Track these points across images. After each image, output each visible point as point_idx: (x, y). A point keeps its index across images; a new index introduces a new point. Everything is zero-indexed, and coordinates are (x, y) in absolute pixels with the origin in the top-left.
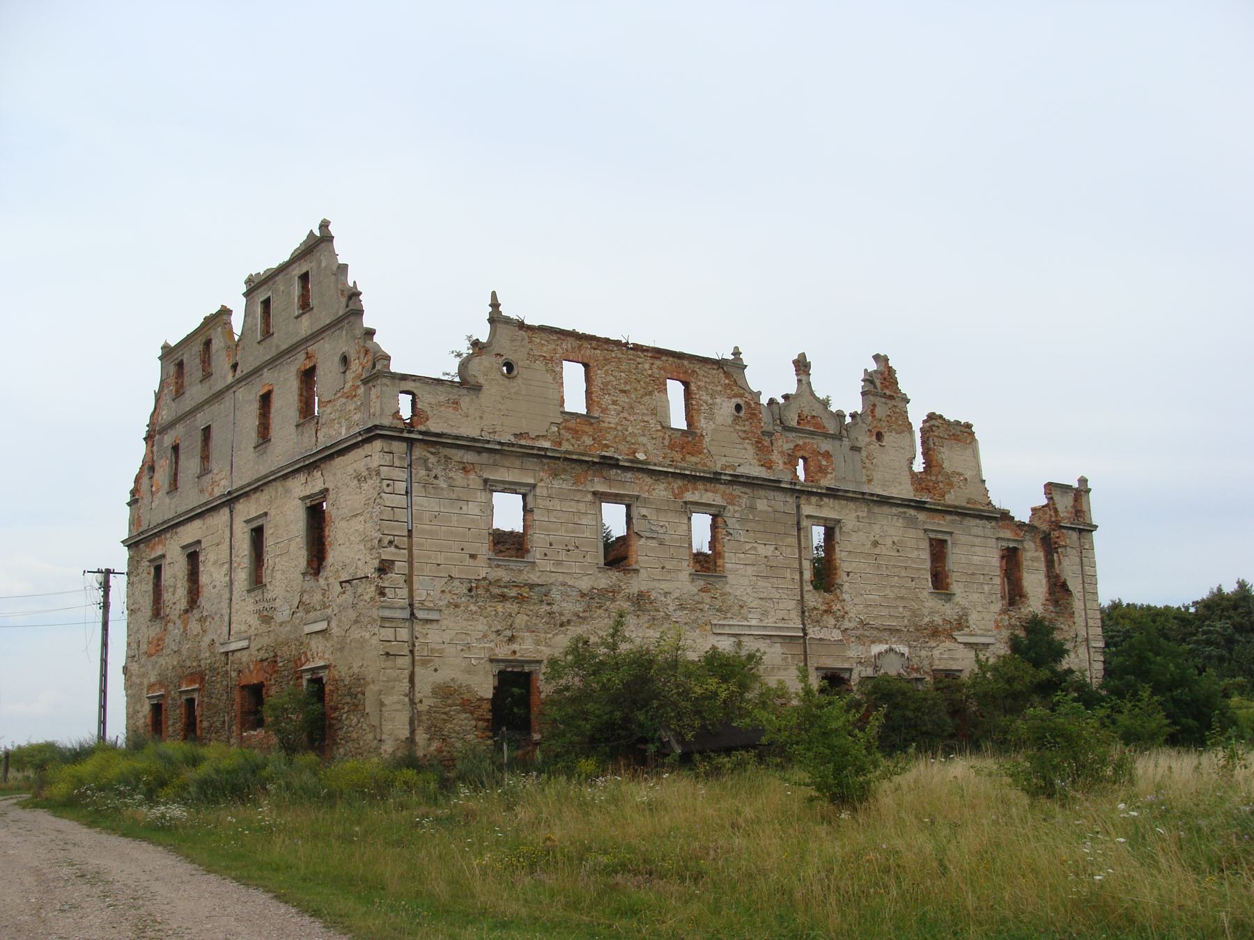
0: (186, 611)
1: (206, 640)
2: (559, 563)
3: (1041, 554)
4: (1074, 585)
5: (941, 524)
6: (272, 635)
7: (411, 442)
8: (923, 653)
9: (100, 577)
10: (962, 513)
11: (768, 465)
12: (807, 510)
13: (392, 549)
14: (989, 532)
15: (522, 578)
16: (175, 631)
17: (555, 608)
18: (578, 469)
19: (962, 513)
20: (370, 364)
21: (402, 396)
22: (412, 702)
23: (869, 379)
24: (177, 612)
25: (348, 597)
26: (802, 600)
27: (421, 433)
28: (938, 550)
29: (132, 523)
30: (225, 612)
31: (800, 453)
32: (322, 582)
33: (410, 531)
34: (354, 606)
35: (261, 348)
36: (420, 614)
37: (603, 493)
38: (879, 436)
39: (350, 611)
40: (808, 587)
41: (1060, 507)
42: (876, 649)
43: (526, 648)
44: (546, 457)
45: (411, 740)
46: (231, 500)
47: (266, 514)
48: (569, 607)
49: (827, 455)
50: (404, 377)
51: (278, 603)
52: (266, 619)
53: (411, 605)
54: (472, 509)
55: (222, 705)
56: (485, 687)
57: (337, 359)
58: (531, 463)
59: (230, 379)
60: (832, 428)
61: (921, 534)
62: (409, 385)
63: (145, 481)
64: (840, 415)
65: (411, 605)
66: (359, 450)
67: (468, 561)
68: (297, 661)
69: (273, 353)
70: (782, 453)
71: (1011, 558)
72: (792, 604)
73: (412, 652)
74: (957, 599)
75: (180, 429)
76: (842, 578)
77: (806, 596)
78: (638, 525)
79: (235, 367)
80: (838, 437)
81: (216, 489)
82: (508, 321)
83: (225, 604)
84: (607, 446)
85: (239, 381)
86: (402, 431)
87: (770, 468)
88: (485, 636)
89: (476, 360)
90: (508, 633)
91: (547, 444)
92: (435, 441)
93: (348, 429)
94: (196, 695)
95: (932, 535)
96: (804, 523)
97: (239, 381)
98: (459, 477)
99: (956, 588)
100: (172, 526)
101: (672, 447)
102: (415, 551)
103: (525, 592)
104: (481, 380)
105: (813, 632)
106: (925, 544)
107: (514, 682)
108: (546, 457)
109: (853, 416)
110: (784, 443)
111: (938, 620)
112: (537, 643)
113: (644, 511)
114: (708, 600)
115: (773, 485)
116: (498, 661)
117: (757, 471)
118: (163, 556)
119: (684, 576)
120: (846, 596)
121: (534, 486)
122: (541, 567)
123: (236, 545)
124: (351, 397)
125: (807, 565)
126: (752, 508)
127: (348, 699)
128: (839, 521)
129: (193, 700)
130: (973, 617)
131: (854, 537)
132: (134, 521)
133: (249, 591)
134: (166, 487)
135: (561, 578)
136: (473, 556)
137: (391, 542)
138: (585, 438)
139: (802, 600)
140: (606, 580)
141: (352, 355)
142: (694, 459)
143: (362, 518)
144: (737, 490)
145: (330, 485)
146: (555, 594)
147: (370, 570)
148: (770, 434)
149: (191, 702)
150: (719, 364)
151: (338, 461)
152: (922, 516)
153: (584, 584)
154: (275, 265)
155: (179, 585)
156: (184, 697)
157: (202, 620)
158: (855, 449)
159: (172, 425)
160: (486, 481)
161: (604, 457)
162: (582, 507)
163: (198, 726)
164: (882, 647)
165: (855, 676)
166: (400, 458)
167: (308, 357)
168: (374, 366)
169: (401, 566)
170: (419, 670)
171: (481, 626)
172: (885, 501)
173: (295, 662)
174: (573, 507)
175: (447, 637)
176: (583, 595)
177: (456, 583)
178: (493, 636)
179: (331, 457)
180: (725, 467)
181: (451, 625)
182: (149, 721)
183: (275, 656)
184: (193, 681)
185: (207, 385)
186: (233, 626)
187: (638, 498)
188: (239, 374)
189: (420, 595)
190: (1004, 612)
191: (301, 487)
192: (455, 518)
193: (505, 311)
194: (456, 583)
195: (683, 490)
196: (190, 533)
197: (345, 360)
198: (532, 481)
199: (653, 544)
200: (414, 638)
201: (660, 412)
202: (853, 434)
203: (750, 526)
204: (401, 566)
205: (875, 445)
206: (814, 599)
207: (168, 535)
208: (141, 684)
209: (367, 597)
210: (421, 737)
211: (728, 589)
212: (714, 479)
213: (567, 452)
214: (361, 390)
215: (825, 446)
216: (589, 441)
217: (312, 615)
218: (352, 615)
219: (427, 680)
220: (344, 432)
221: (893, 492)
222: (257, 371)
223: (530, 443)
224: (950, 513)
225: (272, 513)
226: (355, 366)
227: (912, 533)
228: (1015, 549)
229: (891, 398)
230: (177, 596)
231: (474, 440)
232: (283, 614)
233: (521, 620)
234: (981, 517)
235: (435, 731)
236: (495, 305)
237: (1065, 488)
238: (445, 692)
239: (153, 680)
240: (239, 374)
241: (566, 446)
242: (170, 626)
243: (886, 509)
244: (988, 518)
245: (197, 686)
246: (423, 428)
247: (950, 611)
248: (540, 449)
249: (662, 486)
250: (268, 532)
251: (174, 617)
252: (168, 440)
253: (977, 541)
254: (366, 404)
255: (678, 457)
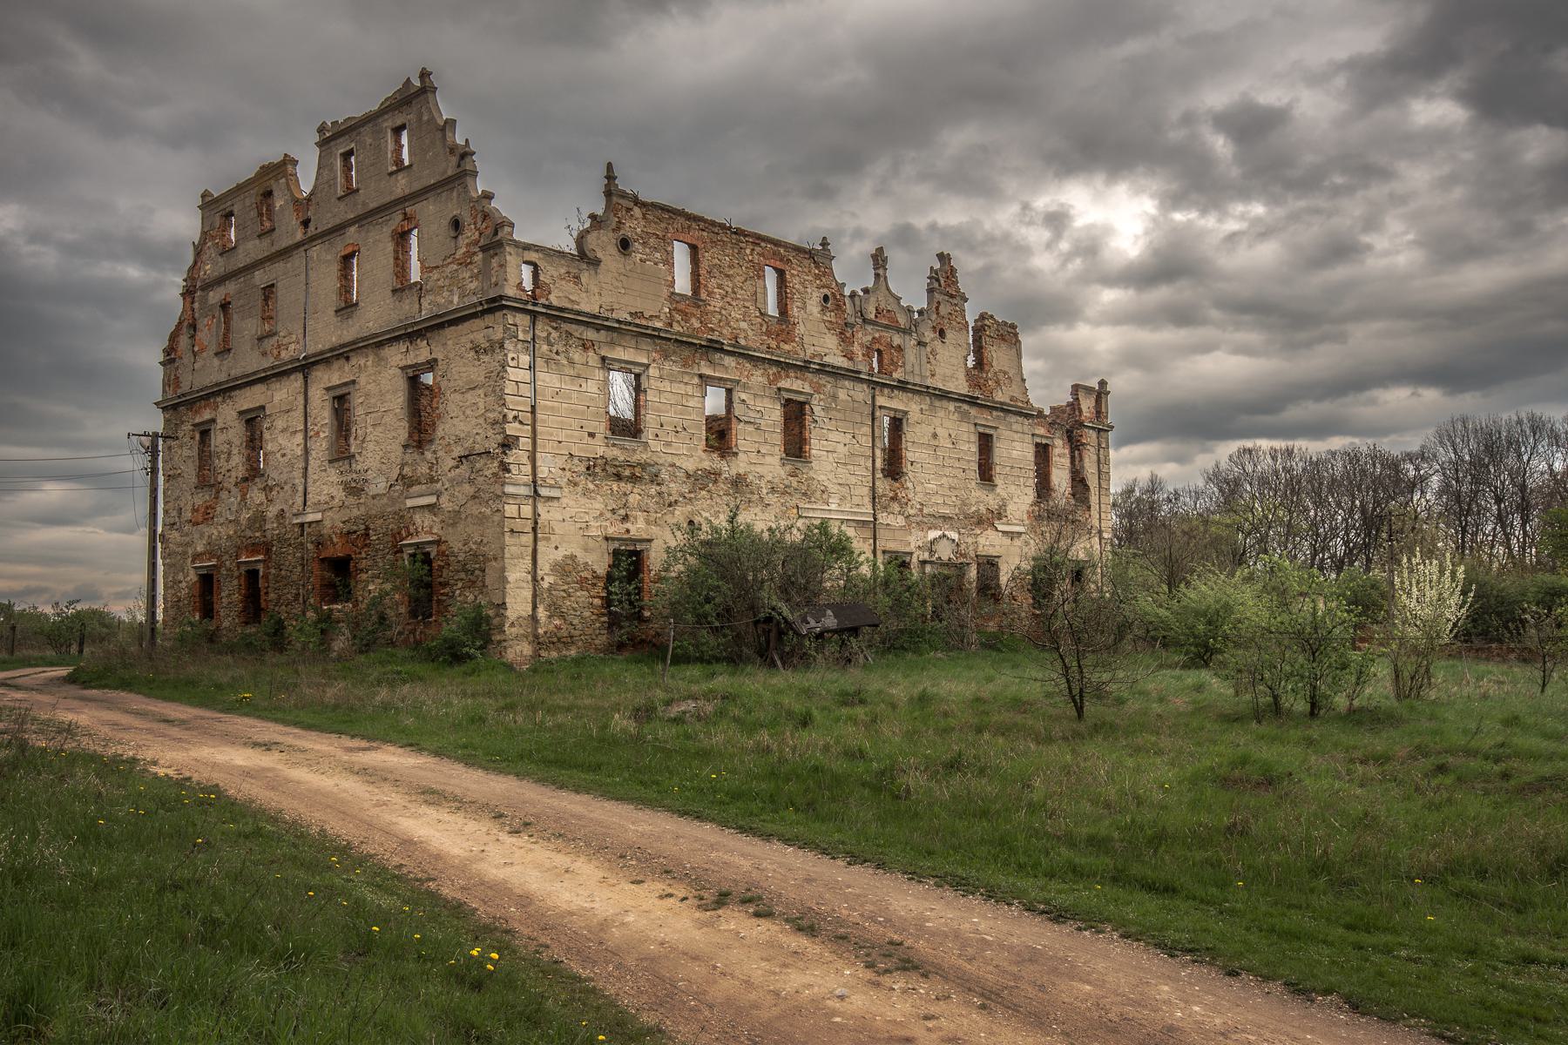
0: (246, 479)
1: (272, 512)
2: (668, 444)
3: (1067, 451)
4: (1092, 482)
5: (985, 418)
6: (362, 509)
7: (534, 315)
8: (970, 540)
9: (147, 441)
10: (1004, 409)
11: (849, 356)
12: (881, 401)
13: (517, 425)
14: (1026, 429)
15: (635, 458)
16: (231, 500)
17: (664, 488)
18: (687, 352)
19: (1004, 409)
20: (489, 231)
21: (524, 267)
22: (535, 579)
23: (934, 276)
24: (233, 480)
25: (464, 469)
26: (873, 488)
27: (544, 306)
28: (985, 443)
29: (166, 383)
30: (299, 481)
31: (877, 346)
32: (429, 455)
33: (533, 407)
34: (471, 481)
35: (342, 205)
36: (543, 492)
37: (709, 377)
38: (942, 333)
39: (467, 486)
40: (879, 475)
41: (1084, 407)
42: (933, 534)
43: (638, 528)
44: (659, 337)
45: (534, 618)
46: (305, 367)
47: (353, 382)
48: (674, 488)
49: (900, 349)
50: (527, 247)
51: (370, 475)
52: (354, 490)
53: (534, 482)
54: (592, 387)
55: (295, 577)
56: (599, 563)
57: (445, 222)
58: (646, 344)
59: (299, 236)
60: (902, 321)
61: (972, 428)
62: (533, 256)
63: (184, 341)
64: (909, 310)
65: (534, 482)
66: (477, 321)
67: (587, 439)
68: (397, 536)
69: (360, 210)
70: (861, 345)
71: (1043, 453)
72: (866, 491)
73: (534, 529)
74: (998, 490)
75: (231, 287)
76: (907, 468)
77: (878, 483)
78: (738, 410)
79: (306, 223)
80: (905, 332)
81: (283, 354)
82: (623, 195)
83: (298, 474)
84: (712, 330)
85: (313, 239)
86: (527, 303)
87: (851, 359)
88: (601, 514)
89: (594, 234)
90: (622, 512)
91: (659, 325)
92: (557, 316)
93: (462, 296)
94: (261, 568)
95: (981, 430)
96: (878, 414)
97: (313, 239)
98: (577, 355)
99: (998, 480)
100: (226, 390)
101: (768, 333)
102: (539, 429)
103: (638, 472)
104: (600, 255)
105: (883, 518)
106: (974, 438)
107: (629, 560)
108: (659, 337)
109: (921, 312)
110: (863, 336)
111: (983, 510)
112: (648, 522)
113: (743, 396)
114: (795, 484)
115: (853, 376)
116: (613, 539)
117: (840, 361)
118: (213, 421)
119: (775, 460)
120: (909, 485)
121: (648, 366)
122: (655, 447)
123: (313, 411)
124: (465, 263)
125: (878, 453)
126: (835, 397)
127: (463, 575)
128: (906, 413)
129: (256, 572)
130: (1011, 508)
131: (917, 429)
132: (171, 382)
133: (330, 462)
134: (213, 348)
135: (670, 459)
136: (592, 435)
137: (515, 418)
138: (693, 320)
139: (873, 488)
140: (710, 462)
141: (467, 218)
142: (787, 347)
143: (481, 392)
144: (824, 379)
145: (440, 356)
146: (664, 475)
147: (492, 446)
148: (852, 326)
149: (252, 575)
150: (810, 254)
151: (450, 332)
152: (973, 411)
153: (690, 465)
154: (359, 114)
155: (235, 451)
156: (243, 569)
157: (267, 489)
158: (920, 343)
159: (221, 281)
160: (603, 359)
161: (711, 341)
162: (689, 389)
163: (263, 597)
164: (937, 533)
165: (914, 560)
166: (525, 332)
167: (406, 218)
168: (496, 233)
169: (525, 443)
170: (541, 546)
171: (598, 505)
172: (944, 396)
173: (394, 536)
174: (681, 389)
175: (567, 514)
176: (688, 476)
177: (576, 461)
178: (609, 515)
179: (441, 326)
180: (814, 356)
181: (572, 503)
182: (196, 592)
183: (367, 529)
184: (254, 552)
185: (266, 242)
186: (309, 496)
187: (738, 382)
188: (312, 230)
189: (543, 472)
190: (1034, 504)
191: (397, 356)
192: (575, 395)
193: (621, 185)
194: (576, 461)
195: (777, 377)
196: (249, 399)
197: (456, 224)
198: (645, 361)
199: (750, 428)
200: (536, 515)
201: (757, 297)
202: (921, 329)
203: (833, 414)
204: (525, 443)
205: (938, 343)
206: (883, 486)
207: (219, 399)
208: (185, 553)
209: (488, 473)
210: (542, 613)
211: (811, 474)
212: (804, 368)
213: (678, 333)
214: (479, 257)
215: (897, 340)
216: (697, 325)
217: (416, 489)
218: (469, 489)
219: (549, 555)
220: (456, 299)
221: (950, 387)
222: (339, 229)
223: (644, 322)
224: (996, 409)
225: (362, 380)
226: (470, 234)
227: (965, 427)
228: (1047, 446)
229: (952, 296)
230: (233, 463)
231: (595, 317)
232: (378, 486)
233: (633, 499)
234: (1020, 414)
235: (555, 610)
236: (610, 177)
237: (1089, 390)
238: (565, 568)
239: (200, 549)
240: (312, 230)
241: (676, 327)
242: (224, 495)
243: (945, 403)
244: (1027, 416)
245: (261, 557)
246: (543, 301)
247: (992, 501)
248: (654, 329)
249: (759, 372)
250: (357, 400)
251: (229, 483)
252: (215, 296)
253: (1016, 436)
254: (484, 273)
255: (774, 344)
